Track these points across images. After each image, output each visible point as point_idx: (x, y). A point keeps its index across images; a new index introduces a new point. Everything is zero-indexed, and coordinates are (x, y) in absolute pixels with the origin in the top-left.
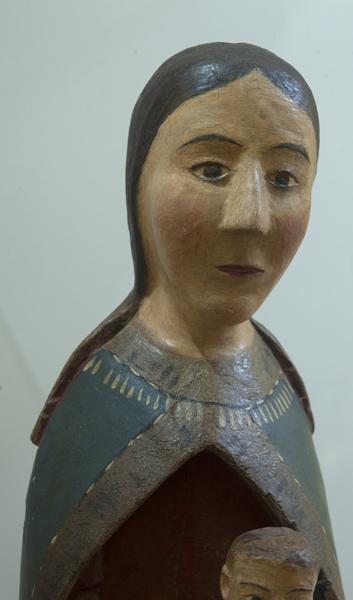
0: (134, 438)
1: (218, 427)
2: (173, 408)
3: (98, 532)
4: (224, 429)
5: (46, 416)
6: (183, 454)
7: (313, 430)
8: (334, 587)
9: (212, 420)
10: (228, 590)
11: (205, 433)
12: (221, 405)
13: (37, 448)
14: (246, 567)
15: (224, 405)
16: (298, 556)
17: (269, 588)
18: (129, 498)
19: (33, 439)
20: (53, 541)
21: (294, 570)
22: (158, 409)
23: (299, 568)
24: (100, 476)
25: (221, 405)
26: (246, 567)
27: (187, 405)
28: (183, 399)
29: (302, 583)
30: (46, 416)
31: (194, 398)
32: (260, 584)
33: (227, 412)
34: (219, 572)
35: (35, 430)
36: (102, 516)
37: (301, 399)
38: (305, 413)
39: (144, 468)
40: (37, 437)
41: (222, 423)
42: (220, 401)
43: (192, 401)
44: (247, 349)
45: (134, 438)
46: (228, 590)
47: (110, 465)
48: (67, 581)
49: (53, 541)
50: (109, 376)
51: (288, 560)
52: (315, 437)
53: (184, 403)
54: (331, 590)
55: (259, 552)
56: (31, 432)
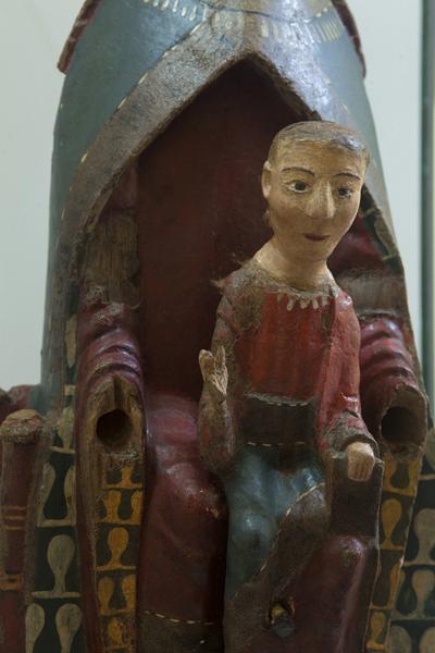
0: (169, 49)
1: (260, 36)
2: (210, 19)
3: (133, 142)
4: (267, 39)
5: (73, 40)
6: (221, 62)
7: (364, 73)
8: (384, 216)
9: (252, 29)
10: (269, 187)
11: (246, 41)
12: (263, 14)
13: (64, 76)
14: (290, 152)
15: (267, 16)
16: (345, 139)
17: (313, 171)
18: (165, 106)
19: (59, 66)
20: (83, 160)
21: (340, 151)
22: (195, 19)
23: (346, 150)
24: (132, 91)
25: (263, 14)
26: (290, 152)
27: (226, 15)
28: (222, 8)
29: (349, 167)
30: (73, 40)
31: (234, 7)
32: (304, 167)
33: (270, 22)
34: (260, 169)
35: (63, 55)
36: (135, 128)
37: (352, 38)
38: (354, 53)
39: (178, 78)
40: (64, 65)
41: (265, 32)
42: (263, 12)
43: (233, 10)
44: (389, 328)
45: (169, 49)
46: (269, 187)
47: (143, 78)
48: (99, 194)
49: (83, 160)
50: (383, 312)
51: (334, 141)
52: (367, 82)
53: (223, 12)
54: (381, 219)
55: (302, 134)
56: (57, 60)
